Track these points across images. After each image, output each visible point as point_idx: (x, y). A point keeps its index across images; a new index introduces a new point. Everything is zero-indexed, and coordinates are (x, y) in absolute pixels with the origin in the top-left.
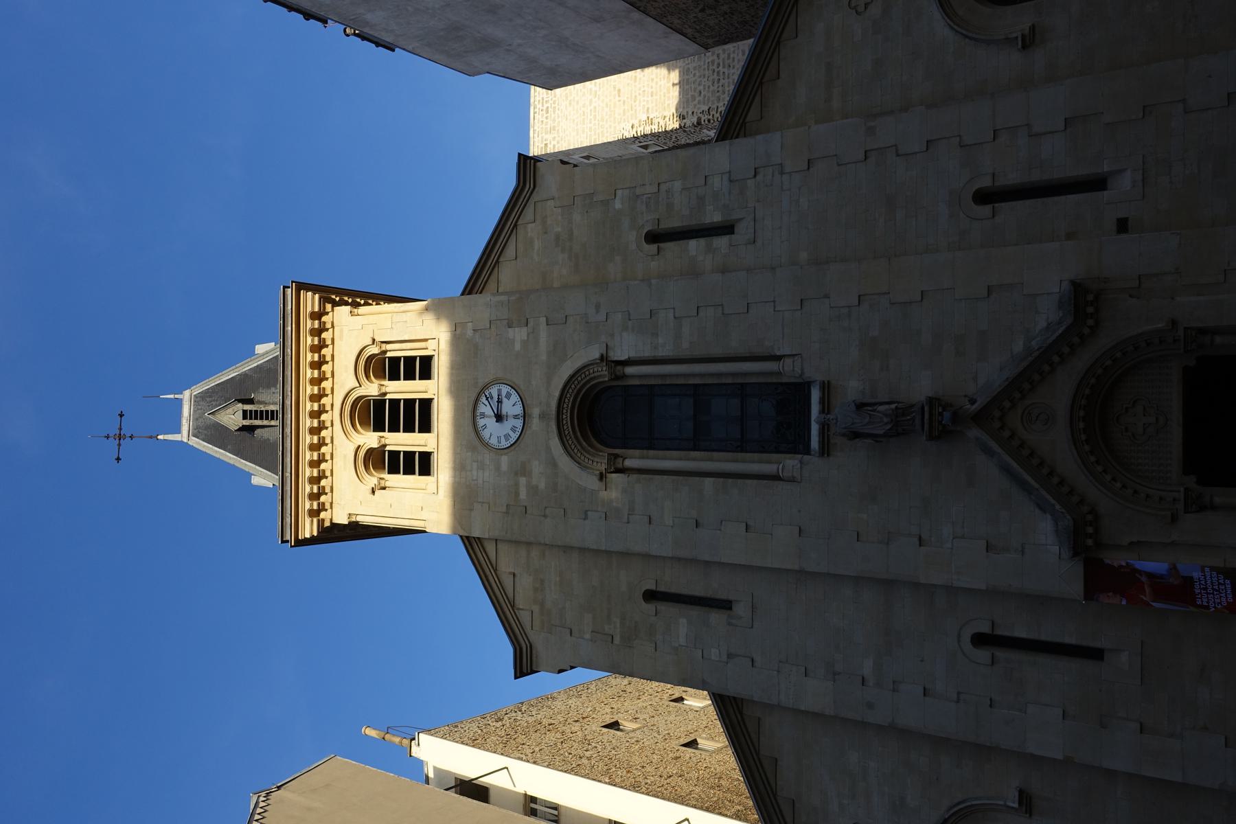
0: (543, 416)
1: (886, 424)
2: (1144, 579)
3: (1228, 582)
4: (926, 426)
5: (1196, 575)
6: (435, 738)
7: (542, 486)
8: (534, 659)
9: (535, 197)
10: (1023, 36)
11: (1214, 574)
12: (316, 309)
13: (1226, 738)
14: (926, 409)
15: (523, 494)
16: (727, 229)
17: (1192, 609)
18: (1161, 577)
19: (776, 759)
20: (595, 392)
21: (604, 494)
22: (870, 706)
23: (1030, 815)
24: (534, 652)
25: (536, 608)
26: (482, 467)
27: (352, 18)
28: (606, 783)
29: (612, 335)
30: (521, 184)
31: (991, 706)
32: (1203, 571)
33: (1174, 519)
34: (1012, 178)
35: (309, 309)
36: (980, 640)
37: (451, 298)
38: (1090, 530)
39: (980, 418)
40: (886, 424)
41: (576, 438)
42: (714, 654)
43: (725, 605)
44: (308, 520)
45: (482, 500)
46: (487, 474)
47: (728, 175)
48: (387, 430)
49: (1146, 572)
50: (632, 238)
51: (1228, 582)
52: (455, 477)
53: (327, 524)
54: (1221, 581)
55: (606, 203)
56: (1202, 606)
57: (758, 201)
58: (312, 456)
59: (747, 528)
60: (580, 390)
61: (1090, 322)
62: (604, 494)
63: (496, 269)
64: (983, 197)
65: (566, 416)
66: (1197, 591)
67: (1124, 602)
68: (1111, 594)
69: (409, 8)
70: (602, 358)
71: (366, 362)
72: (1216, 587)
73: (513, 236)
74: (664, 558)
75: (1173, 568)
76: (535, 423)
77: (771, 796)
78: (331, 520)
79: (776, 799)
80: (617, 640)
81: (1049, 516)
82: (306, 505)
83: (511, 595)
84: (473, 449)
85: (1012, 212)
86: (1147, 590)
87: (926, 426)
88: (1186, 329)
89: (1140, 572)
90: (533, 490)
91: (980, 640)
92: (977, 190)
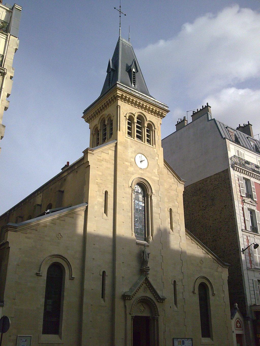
9: (178, 182)
10: (194, 292)
14: (148, 268)
15: (127, 163)
29: (156, 197)
35: (164, 113)
36: (104, 272)
38: (129, 299)
44: (121, 94)
61: (160, 301)
64: (175, 282)
76: (141, 171)
78: (119, 100)
88: (158, 318)
91: (104, 272)
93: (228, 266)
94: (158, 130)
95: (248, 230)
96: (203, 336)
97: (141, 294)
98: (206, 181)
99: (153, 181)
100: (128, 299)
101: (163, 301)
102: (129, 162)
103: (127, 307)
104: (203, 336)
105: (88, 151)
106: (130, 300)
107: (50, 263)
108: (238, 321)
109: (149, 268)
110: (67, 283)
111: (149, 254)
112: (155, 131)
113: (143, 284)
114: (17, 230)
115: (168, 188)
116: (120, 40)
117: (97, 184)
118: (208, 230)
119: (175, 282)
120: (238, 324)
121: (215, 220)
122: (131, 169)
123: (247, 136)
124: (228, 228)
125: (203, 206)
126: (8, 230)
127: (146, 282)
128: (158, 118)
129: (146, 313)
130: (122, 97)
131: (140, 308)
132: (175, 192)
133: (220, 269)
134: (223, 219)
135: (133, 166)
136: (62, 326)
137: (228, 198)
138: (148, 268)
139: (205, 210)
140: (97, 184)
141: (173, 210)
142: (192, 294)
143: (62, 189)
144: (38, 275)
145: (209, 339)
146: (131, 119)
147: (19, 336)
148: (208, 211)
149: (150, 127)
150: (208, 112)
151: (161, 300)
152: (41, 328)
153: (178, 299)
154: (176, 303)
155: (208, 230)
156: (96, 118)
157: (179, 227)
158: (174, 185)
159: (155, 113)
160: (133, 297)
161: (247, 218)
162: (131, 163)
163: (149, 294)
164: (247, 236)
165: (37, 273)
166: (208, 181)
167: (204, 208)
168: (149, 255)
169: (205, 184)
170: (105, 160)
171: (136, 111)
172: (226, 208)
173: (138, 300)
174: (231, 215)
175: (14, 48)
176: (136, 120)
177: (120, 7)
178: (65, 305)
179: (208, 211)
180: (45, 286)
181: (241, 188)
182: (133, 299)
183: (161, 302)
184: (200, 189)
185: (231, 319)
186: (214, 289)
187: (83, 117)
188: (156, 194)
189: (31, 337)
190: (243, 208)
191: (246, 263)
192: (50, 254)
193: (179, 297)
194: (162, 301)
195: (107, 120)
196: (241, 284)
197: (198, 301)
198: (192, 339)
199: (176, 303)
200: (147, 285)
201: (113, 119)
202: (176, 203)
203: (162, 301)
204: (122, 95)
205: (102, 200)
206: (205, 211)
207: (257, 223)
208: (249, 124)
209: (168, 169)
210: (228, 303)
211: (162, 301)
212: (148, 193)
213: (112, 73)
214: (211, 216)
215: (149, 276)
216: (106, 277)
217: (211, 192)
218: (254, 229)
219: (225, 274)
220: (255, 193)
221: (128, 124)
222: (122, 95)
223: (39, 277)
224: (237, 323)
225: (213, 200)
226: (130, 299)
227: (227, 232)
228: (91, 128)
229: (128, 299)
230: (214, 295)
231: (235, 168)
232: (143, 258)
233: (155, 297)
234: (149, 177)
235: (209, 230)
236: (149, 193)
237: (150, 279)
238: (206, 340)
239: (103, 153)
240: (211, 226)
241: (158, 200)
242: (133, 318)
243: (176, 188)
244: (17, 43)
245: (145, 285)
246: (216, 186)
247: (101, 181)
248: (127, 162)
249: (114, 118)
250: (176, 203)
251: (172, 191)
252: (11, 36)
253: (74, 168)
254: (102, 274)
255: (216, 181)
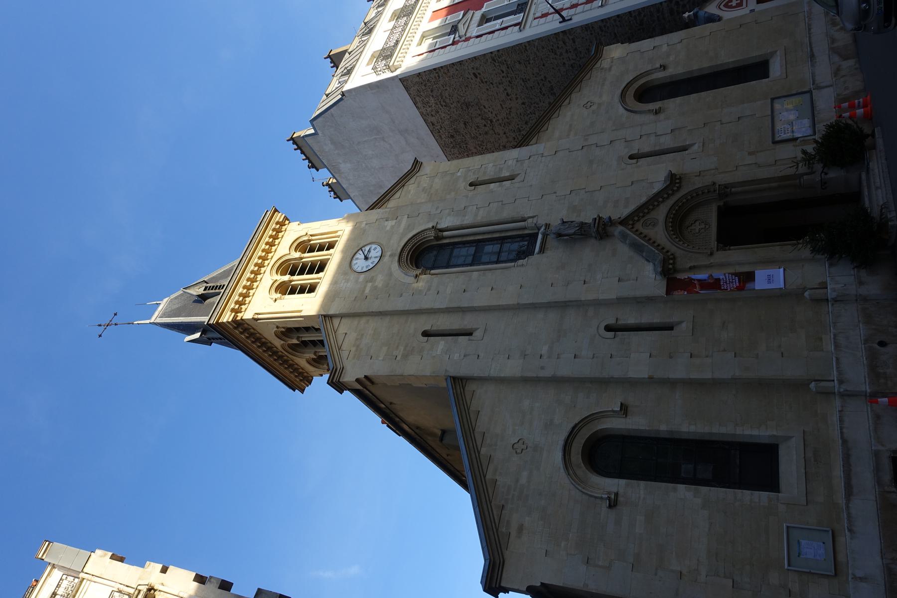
0: (391, 256)
1: (577, 227)
2: (696, 282)
3: (737, 278)
4: (596, 225)
6: (398, 8)
8: (342, 375)
9: (417, 175)
10: (656, 110)
12: (281, 220)
13: (735, 353)
14: (597, 221)
15: (367, 290)
16: (511, 178)
17: (719, 291)
18: (705, 280)
20: (425, 246)
21: (415, 285)
22: (542, 368)
23: (626, 416)
24: (344, 371)
25: (353, 349)
26: (347, 281)
27: (334, 164)
29: (441, 219)
30: (413, 168)
31: (611, 358)
32: (725, 274)
33: (712, 254)
34: (646, 149)
35: (277, 219)
36: (608, 328)
38: (671, 261)
39: (623, 222)
40: (577, 227)
42: (456, 356)
43: (469, 334)
44: (229, 313)
46: (349, 284)
49: (697, 280)
50: (462, 185)
51: (737, 278)
52: (329, 287)
53: (239, 318)
54: (734, 278)
55: (453, 174)
56: (724, 289)
57: (529, 167)
58: (258, 261)
60: (416, 243)
61: (677, 185)
62: (415, 285)
63: (387, 203)
64: (631, 157)
65: (405, 254)
66: (722, 284)
67: (686, 293)
68: (679, 291)
69: (363, 165)
70: (433, 227)
71: (298, 245)
72: (731, 281)
73: (401, 190)
76: (386, 259)
77: (471, 430)
78: (242, 317)
79: (474, 433)
81: (651, 264)
82: (232, 305)
83: (340, 344)
84: (345, 274)
87: (596, 225)
88: (719, 185)
89: (694, 280)
90: (375, 288)
91: (608, 328)
92: (632, 154)
93: (598, 47)
94: (310, 229)
95: (521, 20)
96: (766, 76)
97: (659, 233)
98: (433, 124)
99: (409, 228)
100: (674, 261)
101: (678, 177)
102: (365, 287)
103: (692, 264)
104: (766, 76)
105: (334, 381)
106: (674, 258)
107: (583, 471)
108: (724, 6)
109: (597, 219)
110: (636, 423)
111: (564, 222)
112: (311, 236)
113: (634, 229)
114: (498, 562)
115: (428, 195)
116: (155, 322)
117: (405, 356)
118: (533, 108)
119: (631, 157)
120: (732, 5)
121: (508, 94)
122: (380, 281)
123: (347, 54)
124: (520, 63)
125: (485, 126)
126: (497, 586)
127: (631, 222)
128: (286, 232)
129: (711, 215)
130: (236, 311)
131: (697, 231)
132: (437, 180)
133: (605, 63)
134: (503, 77)
135: (374, 277)
136: (751, 436)
137: (457, 70)
138: (597, 221)
139: (491, 121)
140: (405, 356)
141: (472, 178)
142: (662, 116)
143: (439, 433)
144: (613, 504)
145: (771, 61)
146: (286, 289)
147: (789, 565)
148: (492, 113)
149: (304, 246)
150: (302, 136)
151: (674, 181)
152: (763, 497)
153: (672, 145)
154: (684, 149)
155: (533, 108)
156: (297, 364)
157: (510, 162)
158: (422, 183)
159: (275, 237)
160: (668, 252)
161: (498, 25)
162: (367, 282)
163: (661, 213)
164: (535, 19)
165: (610, 506)
166: (433, 119)
167: (487, 122)
168: (565, 222)
169: (440, 127)
170: (357, 339)
171: (269, 278)
172: (479, 74)
173: (677, 238)
174: (494, 60)
175: (109, 562)
176: (287, 278)
177: (116, 324)
178: (692, 428)
179: (492, 113)
180: (642, 484)
181: (437, 47)
182: (673, 249)
183: (680, 183)
184: (452, 136)
185: (720, 19)
186: (649, 68)
187: (302, 391)
188: (436, 220)
189: (788, 527)
190: (477, 37)
191: (591, 10)
192: (562, 470)
193: (667, 142)
194: (678, 181)
195: (290, 340)
196: (640, 13)
197: (678, 100)
198: (773, 100)
199: (684, 149)
200: (638, 220)
201: (283, 328)
202: (459, 174)
203: (678, 181)
204: (233, 310)
205: (441, 344)
206: (494, 121)
207: (508, 3)
208: (329, 56)
209: (389, 200)
210: (682, 34)
211: (678, 179)
212: (433, 238)
213: (210, 335)
214: (501, 105)
215: (615, 217)
216: (620, 322)
217: (454, 112)
218: (521, 8)
219: (615, 52)
220: (448, 18)
221: (294, 293)
222: (233, 310)
223: (621, 499)
224: (731, 7)
225: (468, 105)
226: (672, 259)
227: (529, 63)
228: (321, 373)
229: (674, 264)
230: (663, 67)
231: (398, 63)
232: (574, 234)
233: (668, 198)
234: (401, 239)
235: (530, 107)
236: (431, 236)
237: (625, 212)
238: (776, 68)
239: (344, 347)
240: (523, 103)
241: (449, 215)
242: (721, 245)
243: (428, 178)
244: (101, 556)
245: (639, 226)
246: (440, 102)
247: (401, 348)
248: (364, 291)
249: (280, 326)
250: (458, 175)
251: (434, 186)
252: (85, 570)
253: (385, 408)
254: (611, 334)
255: (428, 103)
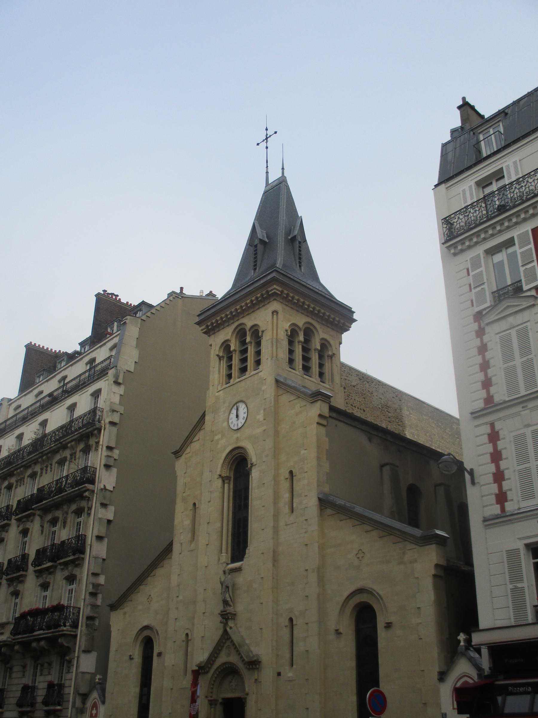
2: (196, 688)
5: (197, 704)
7: (219, 446)
11: (197, 709)
19: (163, 567)
28: (305, 315)
37: (535, 274)
41: (232, 458)
45: (496, 133)
47: (285, 398)
48: (527, 465)
59: (207, 545)
74: (195, 526)
75: (198, 697)
80: (184, 494)
83: (194, 440)
85: (285, 633)
86: (194, 689)
89: (197, 687)
